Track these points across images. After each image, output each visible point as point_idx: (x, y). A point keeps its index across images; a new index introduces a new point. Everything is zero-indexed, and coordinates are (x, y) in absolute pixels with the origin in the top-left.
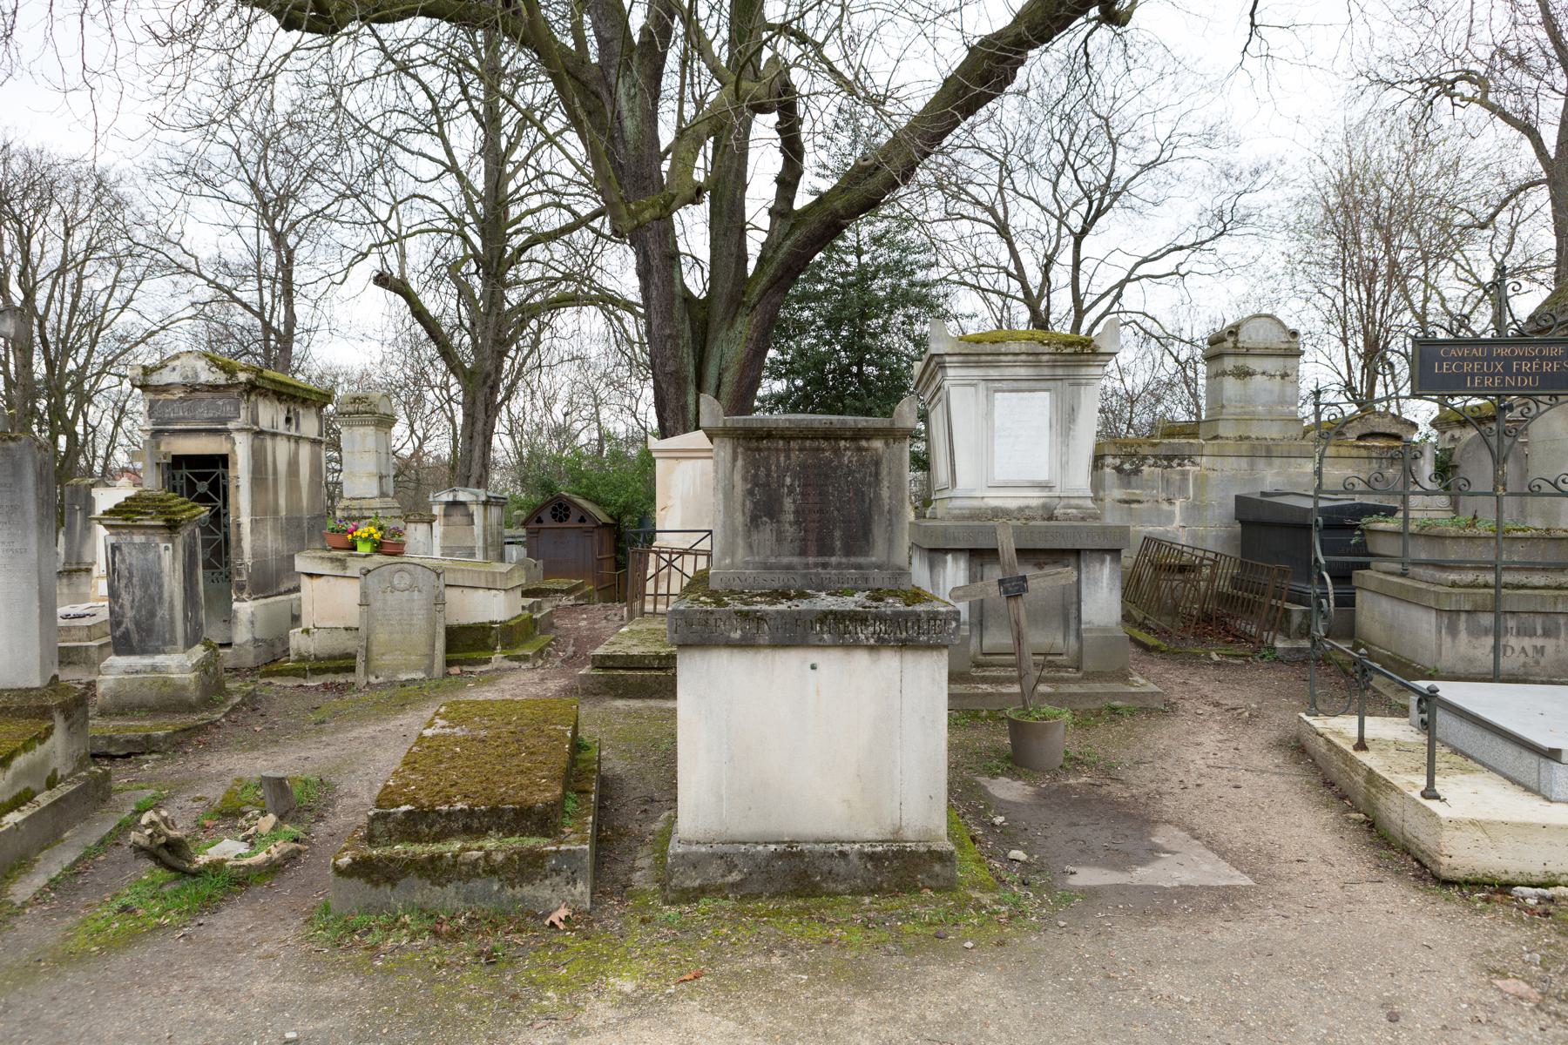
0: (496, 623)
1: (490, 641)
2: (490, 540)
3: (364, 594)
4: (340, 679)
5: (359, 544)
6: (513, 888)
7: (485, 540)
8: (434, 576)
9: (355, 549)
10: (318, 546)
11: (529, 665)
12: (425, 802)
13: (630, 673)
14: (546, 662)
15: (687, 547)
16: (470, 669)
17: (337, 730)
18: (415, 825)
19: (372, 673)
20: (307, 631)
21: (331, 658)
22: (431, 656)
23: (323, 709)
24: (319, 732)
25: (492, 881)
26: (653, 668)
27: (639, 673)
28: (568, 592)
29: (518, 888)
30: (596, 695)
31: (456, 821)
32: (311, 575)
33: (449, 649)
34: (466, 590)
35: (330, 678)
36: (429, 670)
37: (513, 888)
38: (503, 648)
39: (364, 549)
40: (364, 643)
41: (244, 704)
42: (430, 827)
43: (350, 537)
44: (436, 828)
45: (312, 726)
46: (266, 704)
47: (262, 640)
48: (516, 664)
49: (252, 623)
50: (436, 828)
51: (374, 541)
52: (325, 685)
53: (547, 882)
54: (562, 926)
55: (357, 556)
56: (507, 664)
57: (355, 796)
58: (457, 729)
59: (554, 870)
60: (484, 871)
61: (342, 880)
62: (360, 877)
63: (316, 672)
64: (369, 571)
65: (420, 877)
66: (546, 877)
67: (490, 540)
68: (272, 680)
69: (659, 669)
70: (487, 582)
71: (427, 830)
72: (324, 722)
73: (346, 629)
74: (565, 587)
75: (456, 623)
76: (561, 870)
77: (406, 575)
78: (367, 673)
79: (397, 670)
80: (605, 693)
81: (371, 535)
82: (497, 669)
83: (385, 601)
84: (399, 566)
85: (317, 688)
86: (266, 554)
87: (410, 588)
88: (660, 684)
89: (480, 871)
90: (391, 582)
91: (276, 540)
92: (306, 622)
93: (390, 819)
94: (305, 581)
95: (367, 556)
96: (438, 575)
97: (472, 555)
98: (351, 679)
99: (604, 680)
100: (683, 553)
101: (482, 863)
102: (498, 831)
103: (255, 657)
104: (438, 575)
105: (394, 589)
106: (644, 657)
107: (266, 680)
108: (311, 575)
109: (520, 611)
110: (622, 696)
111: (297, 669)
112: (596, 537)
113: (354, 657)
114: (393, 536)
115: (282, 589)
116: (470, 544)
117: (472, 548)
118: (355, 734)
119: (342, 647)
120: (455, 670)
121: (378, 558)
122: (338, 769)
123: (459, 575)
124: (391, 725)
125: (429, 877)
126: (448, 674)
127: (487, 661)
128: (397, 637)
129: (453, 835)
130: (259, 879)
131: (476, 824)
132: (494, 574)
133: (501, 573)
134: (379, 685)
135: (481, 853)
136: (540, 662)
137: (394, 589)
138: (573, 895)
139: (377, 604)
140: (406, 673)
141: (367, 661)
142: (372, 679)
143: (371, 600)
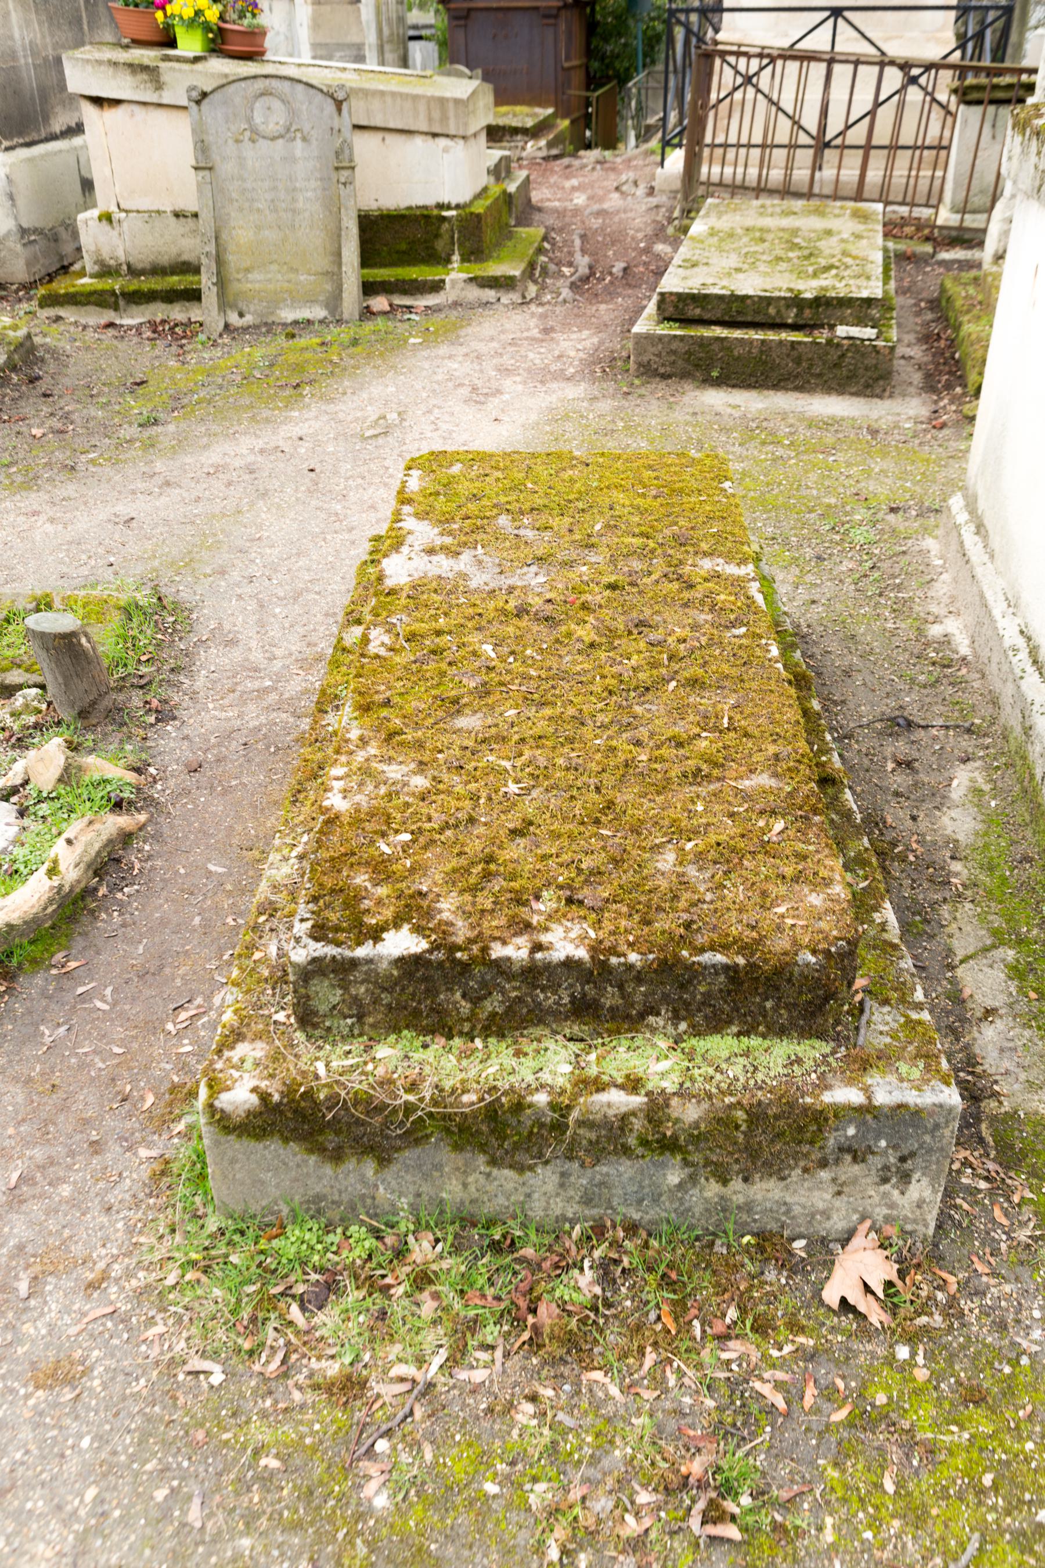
0: (449, 207)
1: (440, 245)
2: (386, 31)
3: (202, 147)
4: (177, 313)
5: (180, 33)
6: (725, 1182)
7: (380, 31)
8: (330, 107)
9: (172, 43)
10: (109, 37)
11: (515, 297)
12: (462, 932)
13: (737, 334)
14: (543, 288)
15: (786, 44)
16: (407, 301)
17: (181, 444)
18: (432, 992)
19: (233, 306)
20: (107, 218)
21: (157, 270)
22: (335, 275)
23: (151, 388)
24: (151, 445)
25: (663, 1165)
26: (783, 326)
27: (757, 335)
28: (534, 132)
29: (737, 1184)
30: (665, 377)
31: (555, 988)
32: (98, 101)
33: (367, 259)
34: (390, 138)
35: (158, 311)
36: (334, 302)
37: (725, 1182)
38: (465, 259)
39: (190, 44)
40: (211, 248)
41: (14, 368)
42: (476, 1001)
43: (159, 15)
44: (493, 1004)
45: (133, 431)
46: (52, 367)
47: (35, 231)
48: (490, 294)
49: (11, 197)
50: (493, 1004)
51: (207, 27)
52: (153, 326)
53: (824, 1175)
54: (876, 1316)
55: (179, 59)
56: (474, 293)
57: (232, 643)
58: (465, 561)
59: (849, 1150)
60: (644, 1143)
61: (236, 1145)
62: (286, 1140)
63: (136, 298)
64: (204, 95)
65: (457, 1147)
66: (823, 1164)
67: (386, 31)
68: (61, 312)
69: (795, 327)
70: (430, 120)
71: (465, 1007)
72: (156, 422)
73: (177, 215)
74: (529, 123)
75: (374, 206)
76: (870, 1151)
77: (276, 104)
78: (224, 304)
79: (276, 301)
80: (684, 375)
81: (632, 1005)
82: (456, 304)
83: (241, 161)
84: (260, 84)
85: (138, 328)
86: (13, 55)
87: (286, 134)
88: (798, 361)
89: (632, 1141)
90: (249, 119)
91: (28, 23)
92: (105, 199)
93: (358, 975)
94: (89, 113)
95: (196, 60)
96: (339, 104)
97: (360, 58)
98: (195, 313)
99: (682, 348)
100: (770, 57)
101: (638, 1124)
102: (676, 1018)
103: (29, 264)
104: (339, 104)
105: (256, 135)
106: (769, 301)
107: (52, 312)
108: (98, 101)
109: (485, 180)
110: (718, 383)
111: (101, 293)
112: (563, 27)
113: (196, 270)
114: (242, 16)
115: (57, 127)
116: (354, 39)
117: (360, 47)
118: (213, 457)
119: (174, 250)
120: (380, 303)
121: (220, 66)
122: (189, 563)
123: (376, 104)
124: (283, 434)
125: (483, 1148)
126: (368, 313)
127: (437, 287)
128: (270, 235)
129: (541, 1021)
130: (35, 950)
131: (610, 998)
132: (442, 101)
133: (457, 101)
134: (246, 329)
135: (637, 1101)
136: (532, 289)
137: (256, 135)
138: (892, 1206)
139: (226, 168)
140: (293, 307)
141: (222, 283)
142: (234, 319)
143: (216, 158)
